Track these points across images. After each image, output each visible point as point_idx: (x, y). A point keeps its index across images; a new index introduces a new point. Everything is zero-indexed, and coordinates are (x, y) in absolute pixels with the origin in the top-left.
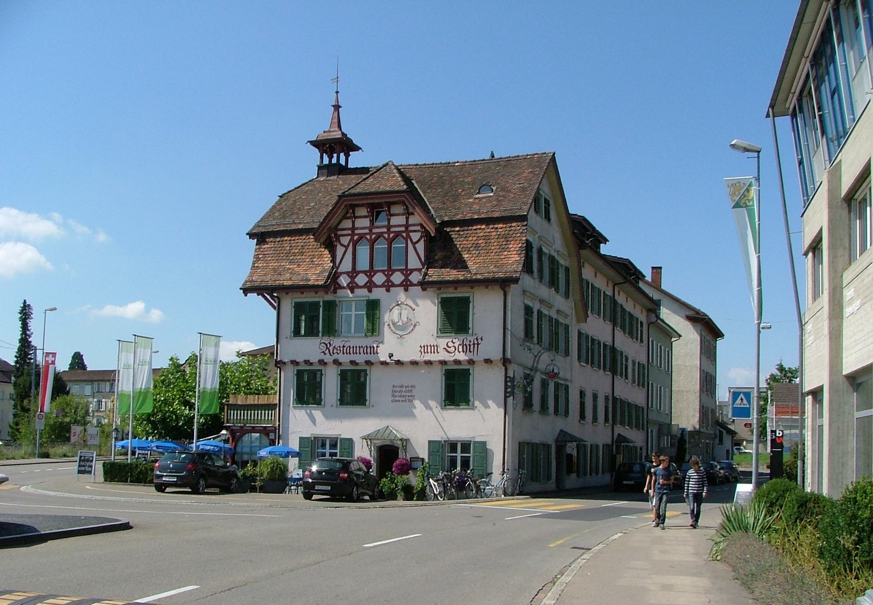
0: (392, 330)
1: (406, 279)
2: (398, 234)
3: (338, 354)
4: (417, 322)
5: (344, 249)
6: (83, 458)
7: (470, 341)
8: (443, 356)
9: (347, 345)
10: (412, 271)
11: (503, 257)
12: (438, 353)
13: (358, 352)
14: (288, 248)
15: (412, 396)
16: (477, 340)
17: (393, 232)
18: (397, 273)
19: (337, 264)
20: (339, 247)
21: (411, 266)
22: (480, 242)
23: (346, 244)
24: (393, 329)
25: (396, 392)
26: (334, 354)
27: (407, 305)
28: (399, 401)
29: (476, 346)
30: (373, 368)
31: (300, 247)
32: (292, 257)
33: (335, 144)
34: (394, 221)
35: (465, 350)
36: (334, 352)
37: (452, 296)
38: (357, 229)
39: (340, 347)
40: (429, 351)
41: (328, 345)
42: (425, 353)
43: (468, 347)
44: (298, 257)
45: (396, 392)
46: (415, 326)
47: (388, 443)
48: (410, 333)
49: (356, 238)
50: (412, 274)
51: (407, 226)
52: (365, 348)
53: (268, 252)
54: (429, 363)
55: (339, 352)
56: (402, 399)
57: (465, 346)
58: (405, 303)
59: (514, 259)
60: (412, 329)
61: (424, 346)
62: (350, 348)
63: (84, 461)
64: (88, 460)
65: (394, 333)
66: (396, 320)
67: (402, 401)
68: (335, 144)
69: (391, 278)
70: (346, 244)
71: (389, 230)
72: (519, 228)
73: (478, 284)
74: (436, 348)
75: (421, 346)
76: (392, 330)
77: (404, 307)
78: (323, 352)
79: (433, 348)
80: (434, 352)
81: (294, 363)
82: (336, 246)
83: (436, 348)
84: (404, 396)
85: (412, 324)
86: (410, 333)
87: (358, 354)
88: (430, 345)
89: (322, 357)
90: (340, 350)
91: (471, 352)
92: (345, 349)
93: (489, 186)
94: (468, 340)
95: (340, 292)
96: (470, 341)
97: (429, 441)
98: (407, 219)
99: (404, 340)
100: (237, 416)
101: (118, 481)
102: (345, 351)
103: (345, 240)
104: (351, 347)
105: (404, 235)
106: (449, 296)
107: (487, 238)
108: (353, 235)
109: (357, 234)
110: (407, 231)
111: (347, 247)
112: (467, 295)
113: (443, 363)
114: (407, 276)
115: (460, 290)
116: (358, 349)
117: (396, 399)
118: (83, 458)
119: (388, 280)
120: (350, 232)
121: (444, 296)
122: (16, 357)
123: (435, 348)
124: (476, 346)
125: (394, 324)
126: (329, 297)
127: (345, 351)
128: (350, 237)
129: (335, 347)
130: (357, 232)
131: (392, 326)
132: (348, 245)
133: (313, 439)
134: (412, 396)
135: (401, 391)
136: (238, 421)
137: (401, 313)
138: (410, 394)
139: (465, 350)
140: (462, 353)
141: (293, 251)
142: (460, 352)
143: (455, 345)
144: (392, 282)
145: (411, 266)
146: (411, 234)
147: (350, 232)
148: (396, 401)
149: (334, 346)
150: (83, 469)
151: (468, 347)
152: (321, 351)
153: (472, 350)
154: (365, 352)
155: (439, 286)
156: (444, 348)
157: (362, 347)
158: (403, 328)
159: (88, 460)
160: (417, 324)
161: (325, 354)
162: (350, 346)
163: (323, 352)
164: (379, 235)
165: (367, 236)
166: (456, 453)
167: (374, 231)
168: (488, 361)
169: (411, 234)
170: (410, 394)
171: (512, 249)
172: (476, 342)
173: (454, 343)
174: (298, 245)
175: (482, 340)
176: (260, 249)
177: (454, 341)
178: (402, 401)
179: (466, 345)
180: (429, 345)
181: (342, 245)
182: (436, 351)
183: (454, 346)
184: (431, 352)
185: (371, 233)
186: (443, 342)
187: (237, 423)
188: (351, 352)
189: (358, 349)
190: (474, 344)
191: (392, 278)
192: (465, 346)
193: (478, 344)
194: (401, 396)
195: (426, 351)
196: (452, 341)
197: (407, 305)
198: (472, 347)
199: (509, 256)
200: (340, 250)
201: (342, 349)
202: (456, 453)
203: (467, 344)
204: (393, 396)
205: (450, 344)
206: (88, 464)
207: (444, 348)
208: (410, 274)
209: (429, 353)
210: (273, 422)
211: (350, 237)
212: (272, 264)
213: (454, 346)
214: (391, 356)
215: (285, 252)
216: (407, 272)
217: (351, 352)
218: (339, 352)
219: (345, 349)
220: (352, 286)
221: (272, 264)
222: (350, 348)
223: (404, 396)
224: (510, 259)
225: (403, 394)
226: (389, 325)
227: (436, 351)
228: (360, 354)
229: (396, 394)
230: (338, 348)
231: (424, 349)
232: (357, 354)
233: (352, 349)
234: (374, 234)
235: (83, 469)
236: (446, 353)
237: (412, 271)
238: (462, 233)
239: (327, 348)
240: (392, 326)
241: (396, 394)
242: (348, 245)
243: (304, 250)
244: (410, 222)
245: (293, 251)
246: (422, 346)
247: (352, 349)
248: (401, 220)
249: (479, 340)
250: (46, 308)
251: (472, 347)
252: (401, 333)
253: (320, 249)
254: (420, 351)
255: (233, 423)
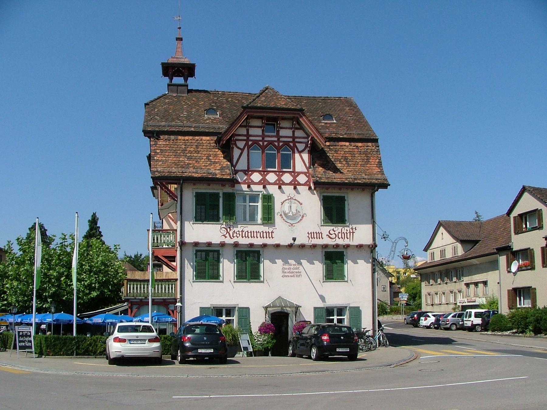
0: (284, 220)
1: (295, 179)
2: (286, 143)
3: (238, 237)
4: (304, 214)
5: (241, 151)
6: (21, 333)
7: (347, 230)
8: (326, 241)
9: (245, 230)
10: (299, 173)
11: (367, 168)
12: (322, 238)
13: (255, 236)
14: (184, 147)
15: (299, 272)
16: (352, 229)
17: (282, 142)
18: (271, 174)
19: (234, 164)
20: (235, 149)
21: (297, 169)
22: (347, 155)
23: (242, 148)
24: (285, 218)
25: (286, 269)
26: (234, 237)
27: (295, 200)
28: (289, 276)
29: (351, 234)
30: (349, 250)
31: (194, 147)
32: (190, 155)
33: (183, 68)
34: (283, 133)
35: (343, 237)
36: (234, 236)
37: (333, 195)
38: (251, 136)
39: (239, 231)
40: (315, 237)
41: (228, 229)
42: (312, 238)
43: (346, 234)
44: (195, 155)
45: (286, 269)
46: (303, 217)
47: (279, 309)
48: (299, 222)
49: (250, 143)
50: (299, 176)
51: (294, 137)
52: (262, 233)
53: (165, 149)
54: (314, 246)
55: (238, 235)
56: (291, 274)
57: (343, 234)
58: (294, 198)
59: (377, 171)
60: (301, 220)
61: (251, 232)
62: (248, 233)
63: (22, 336)
64: (26, 336)
65: (286, 221)
66: (287, 212)
67: (291, 276)
68: (183, 68)
69: (297, 178)
70: (242, 148)
71: (263, 139)
72: (374, 148)
73: (357, 187)
74: (320, 234)
75: (308, 233)
76: (284, 220)
77: (293, 201)
78: (224, 235)
79: (318, 234)
80: (319, 238)
81: (196, 244)
82: (233, 148)
83: (320, 234)
84: (293, 273)
85: (300, 215)
86: (299, 222)
87: (256, 238)
88: (266, 232)
89: (223, 239)
90: (239, 234)
91: (348, 238)
92: (244, 233)
93: (329, 117)
94: (345, 230)
95: (237, 186)
96: (347, 230)
97: (314, 308)
98: (294, 132)
99: (294, 228)
100: (169, 290)
101: (63, 355)
102: (244, 236)
103: (241, 144)
104: (249, 231)
105: (292, 144)
106: (328, 194)
107: (352, 153)
108: (247, 140)
109: (251, 140)
110: (294, 142)
111: (242, 150)
112: (343, 195)
113: (326, 246)
114: (295, 177)
115: (330, 190)
116: (255, 233)
117: (286, 274)
118: (21, 333)
119: (279, 179)
120: (245, 138)
121: (325, 194)
122: (86, 233)
123: (319, 235)
124: (351, 234)
125: (286, 215)
126: (228, 189)
127: (244, 236)
128: (245, 142)
129: (234, 231)
130: (251, 138)
131: (283, 216)
132: (244, 147)
133: (212, 308)
134: (299, 272)
135: (290, 269)
136: (138, 295)
137: (291, 207)
138: (297, 271)
139: (343, 237)
140: (341, 239)
141: (188, 149)
142: (339, 238)
143: (335, 233)
144: (282, 181)
145: (297, 169)
146: (296, 144)
147: (245, 138)
148: (286, 276)
149: (233, 230)
150: (23, 344)
151: (346, 234)
152: (223, 234)
153: (348, 237)
154: (262, 236)
155: (327, 186)
156: (327, 235)
157: (259, 232)
158: (293, 217)
159: (26, 336)
160: (305, 215)
161: (226, 237)
162: (248, 231)
163: (224, 235)
164: (271, 143)
165: (291, 144)
166: (337, 319)
167: (266, 139)
168: (361, 246)
169: (296, 144)
170: (297, 271)
171: (372, 163)
172: (351, 231)
173: (335, 231)
174: (192, 144)
175: (356, 229)
176: (156, 144)
177: (334, 229)
178: (291, 276)
179: (344, 233)
180: (315, 232)
181: (238, 148)
182: (320, 237)
183: (335, 234)
184: (317, 238)
185: (263, 140)
186: (326, 230)
187: (137, 296)
188: (249, 236)
189: (255, 233)
190: (350, 232)
191: (276, 178)
192: (343, 234)
193: (353, 233)
194: (289, 272)
195: (313, 237)
196: (333, 230)
197: (295, 200)
198: (348, 234)
199: (372, 168)
200: (236, 153)
201: (241, 233)
202: (337, 319)
203: (345, 233)
204: (283, 272)
205: (332, 232)
206: (27, 339)
207: (327, 235)
208: (298, 175)
209: (316, 239)
210: (173, 295)
211: (245, 142)
212: (171, 159)
213: (335, 234)
214: (294, 239)
215: (181, 149)
216: (295, 174)
217: (249, 236)
218: (238, 235)
219: (244, 233)
220: (248, 182)
221: (171, 159)
222: (248, 233)
223: (293, 273)
224: (373, 170)
225: (292, 270)
226: (281, 215)
227: (320, 237)
228: (257, 237)
229: (285, 271)
230: (238, 233)
231: (311, 235)
232: (254, 237)
233: (250, 234)
234: (266, 141)
235: (23, 344)
236: (329, 238)
237: (299, 173)
238: (332, 148)
239: (227, 232)
240: (283, 216)
241: (285, 271)
242: (244, 147)
243: (199, 149)
244: (296, 135)
245: (188, 149)
246: (310, 233)
247: (250, 234)
248: (289, 133)
249: (354, 230)
250: (528, 184)
251: (348, 234)
252: (292, 222)
253: (214, 150)
254: (308, 237)
255: (133, 296)
